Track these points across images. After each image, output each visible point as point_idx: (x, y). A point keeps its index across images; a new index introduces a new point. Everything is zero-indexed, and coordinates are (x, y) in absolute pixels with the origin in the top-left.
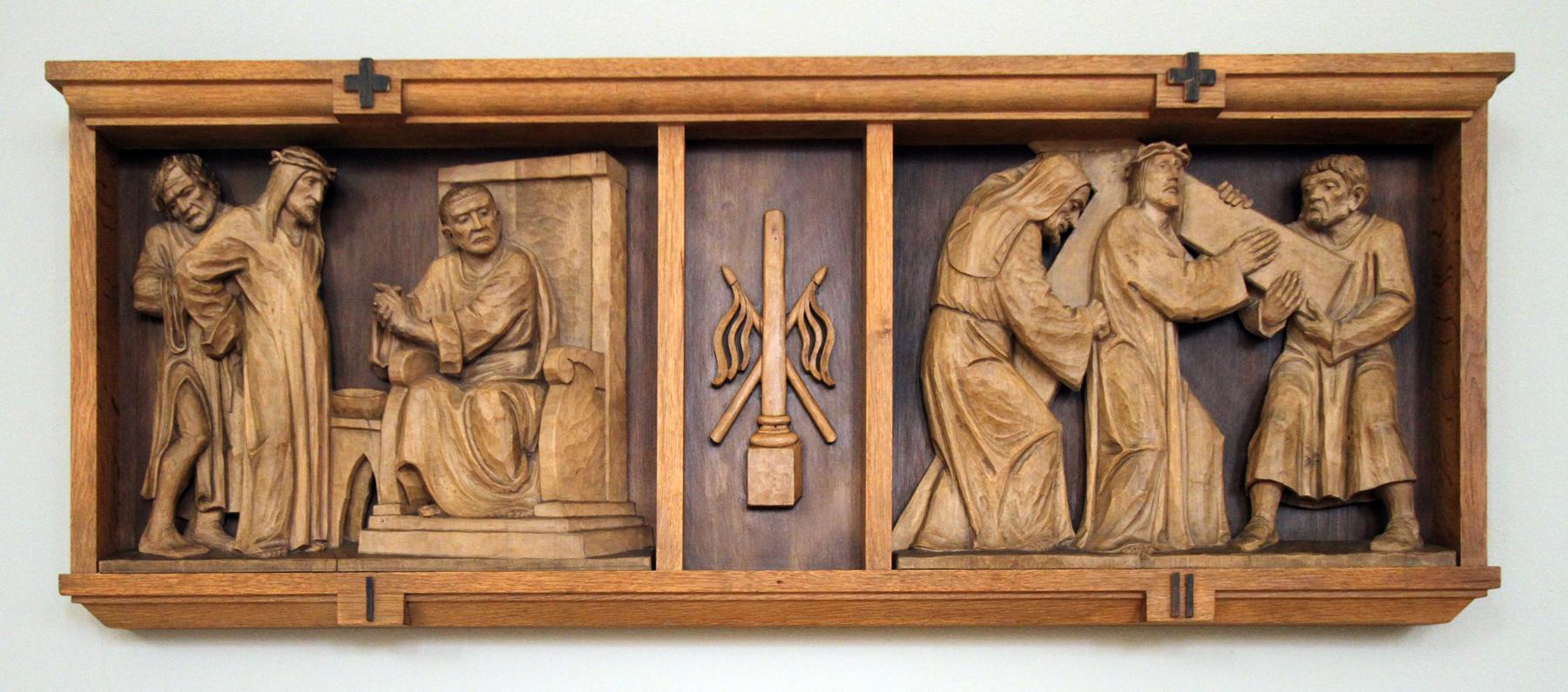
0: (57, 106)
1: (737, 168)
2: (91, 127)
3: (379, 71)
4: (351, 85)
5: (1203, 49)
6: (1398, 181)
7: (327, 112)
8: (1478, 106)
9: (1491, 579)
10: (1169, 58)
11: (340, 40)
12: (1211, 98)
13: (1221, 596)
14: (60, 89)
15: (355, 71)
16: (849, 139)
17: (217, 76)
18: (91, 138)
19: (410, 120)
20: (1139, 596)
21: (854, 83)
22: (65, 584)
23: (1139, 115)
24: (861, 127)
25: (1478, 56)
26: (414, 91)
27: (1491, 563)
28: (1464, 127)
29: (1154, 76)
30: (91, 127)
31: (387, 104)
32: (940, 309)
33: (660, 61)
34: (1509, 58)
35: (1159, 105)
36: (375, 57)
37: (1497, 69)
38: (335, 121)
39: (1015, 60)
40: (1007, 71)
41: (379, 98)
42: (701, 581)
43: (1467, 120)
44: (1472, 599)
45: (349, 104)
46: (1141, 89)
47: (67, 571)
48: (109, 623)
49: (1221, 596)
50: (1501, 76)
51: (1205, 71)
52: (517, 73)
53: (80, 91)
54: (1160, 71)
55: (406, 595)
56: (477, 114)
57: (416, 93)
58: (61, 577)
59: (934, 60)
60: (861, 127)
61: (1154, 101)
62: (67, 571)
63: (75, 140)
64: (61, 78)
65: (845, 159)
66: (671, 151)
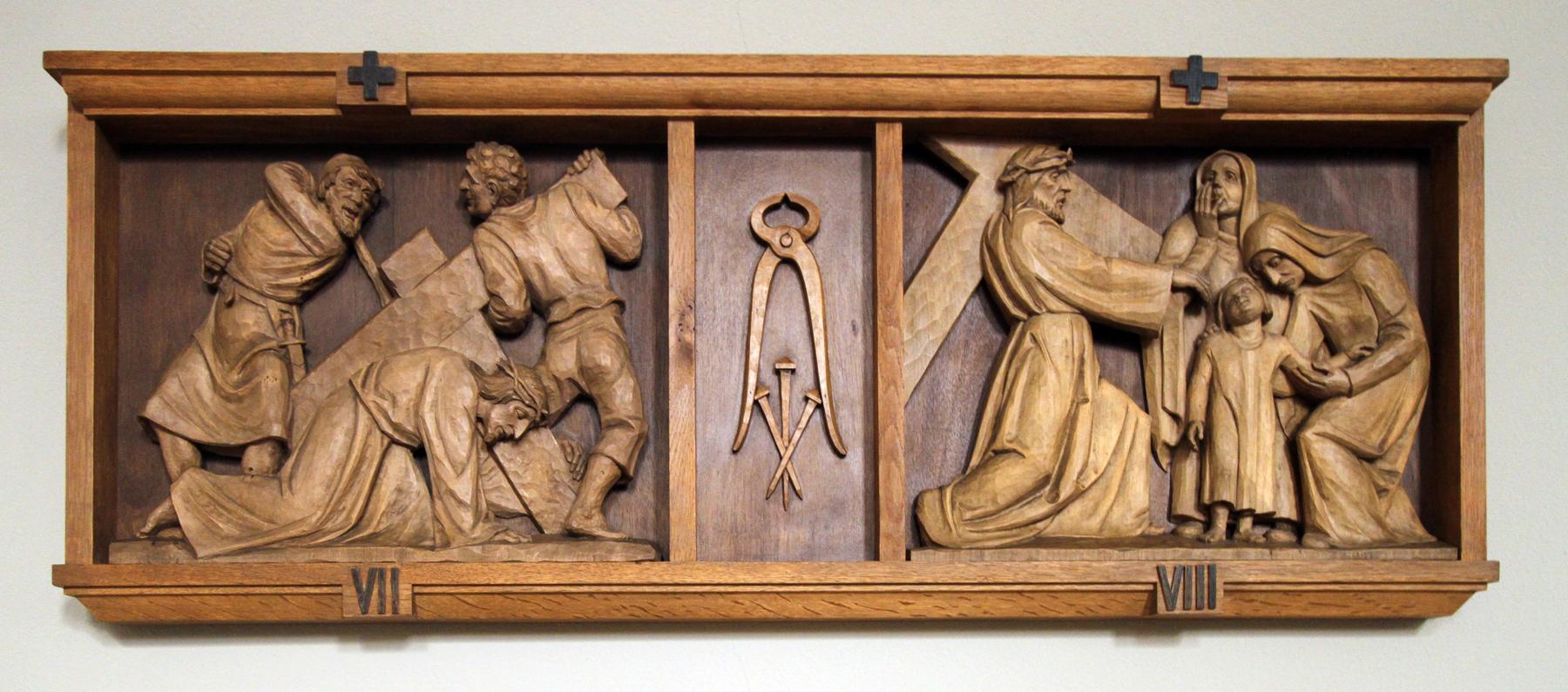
0: (55, 97)
2: (89, 118)
5: (381, 49)
8: (1473, 108)
9: (1493, 572)
11: (339, 33)
13: (417, 590)
14: (59, 80)
15: (359, 63)
18: (90, 132)
19: (414, 112)
20: (1150, 587)
21: (1077, 81)
22: (56, 569)
23: (330, 112)
24: (871, 123)
28: (1461, 130)
29: (1157, 79)
30: (89, 118)
31: (392, 97)
35: (1163, 105)
36: (380, 50)
37: (1495, 75)
38: (339, 113)
39: (125, 56)
40: (860, 70)
43: (1463, 123)
44: (1473, 592)
45: (352, 96)
46: (1145, 91)
49: (417, 590)
50: (1496, 81)
56: (916, 109)
57: (419, 86)
58: (56, 568)
59: (783, 58)
60: (660, 125)
62: (62, 562)
64: (60, 66)
65: (854, 157)
66: (890, 141)
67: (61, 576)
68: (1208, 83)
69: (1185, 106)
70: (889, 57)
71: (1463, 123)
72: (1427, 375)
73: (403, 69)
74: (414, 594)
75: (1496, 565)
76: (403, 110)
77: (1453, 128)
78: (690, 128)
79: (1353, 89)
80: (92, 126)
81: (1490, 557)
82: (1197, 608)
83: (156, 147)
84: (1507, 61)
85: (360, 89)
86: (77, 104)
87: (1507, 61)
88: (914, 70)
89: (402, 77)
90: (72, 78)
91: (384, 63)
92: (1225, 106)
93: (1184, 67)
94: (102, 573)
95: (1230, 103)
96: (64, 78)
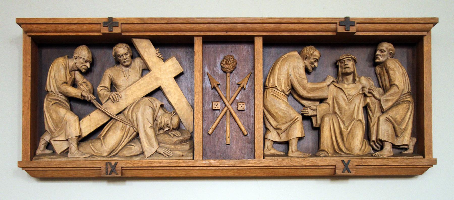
0: (20, 30)
1: (246, 47)
2: (29, 36)
3: (114, 21)
6: (404, 52)
8: (428, 31)
9: (434, 162)
12: (352, 30)
13: (123, 168)
14: (21, 26)
16: (250, 41)
17: (58, 22)
18: (29, 40)
19: (123, 34)
20: (334, 167)
22: (19, 163)
26: (123, 26)
27: (434, 157)
28: (425, 38)
29: (336, 23)
30: (29, 36)
31: (117, 30)
32: (160, 91)
34: (437, 19)
36: (113, 17)
37: (434, 22)
38: (102, 35)
42: (206, 162)
43: (425, 36)
44: (429, 168)
45: (105, 30)
46: (334, 26)
48: (33, 176)
49: (123, 168)
50: (434, 24)
51: (352, 22)
54: (337, 22)
55: (122, 167)
59: (400, 19)
61: (337, 30)
62: (21, 160)
63: (25, 41)
64: (21, 22)
66: (259, 42)
68: (352, 24)
71: (425, 36)
73: (120, 22)
74: (122, 170)
76: (120, 34)
77: (421, 39)
79: (272, 26)
82: (205, 156)
83: (46, 43)
84: (438, 18)
86: (26, 32)
87: (438, 18)
88: (311, 21)
89: (120, 24)
90: (24, 25)
91: (351, 20)
93: (107, 21)
94: (34, 163)
96: (22, 26)
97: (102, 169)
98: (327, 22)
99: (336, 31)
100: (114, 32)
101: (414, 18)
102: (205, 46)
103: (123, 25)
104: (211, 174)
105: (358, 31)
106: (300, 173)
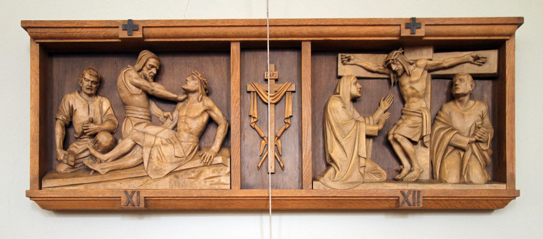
0: (26, 37)
3: (134, 23)
4: (408, 26)
5: (134, 18)
7: (117, 37)
8: (512, 35)
9: (514, 195)
10: (406, 19)
13: (147, 199)
14: (27, 31)
20: (397, 198)
22: (27, 192)
24: (300, 43)
25: (282, 20)
27: (517, 189)
28: (507, 42)
29: (400, 25)
30: (37, 43)
31: (138, 35)
33: (300, 20)
35: (402, 35)
36: (417, 17)
37: (518, 22)
41: (417, 30)
43: (508, 40)
45: (124, 35)
46: (395, 30)
47: (29, 189)
48: (44, 207)
52: (345, 23)
53: (32, 30)
55: (145, 197)
57: (147, 31)
62: (29, 189)
64: (27, 26)
66: (307, 49)
67: (29, 195)
69: (127, 37)
70: (106, 21)
71: (508, 40)
72: (38, 87)
75: (519, 191)
78: (309, 44)
80: (38, 45)
81: (517, 189)
83: (61, 52)
85: (126, 32)
86: (34, 38)
89: (141, 28)
92: (424, 35)
95: (425, 33)
96: (29, 30)
97: (122, 199)
98: (395, 23)
99: (399, 35)
100: (417, 35)
101: (279, 19)
102: (243, 53)
103: (145, 29)
104: (304, 206)
105: (426, 36)
106: (476, 205)
